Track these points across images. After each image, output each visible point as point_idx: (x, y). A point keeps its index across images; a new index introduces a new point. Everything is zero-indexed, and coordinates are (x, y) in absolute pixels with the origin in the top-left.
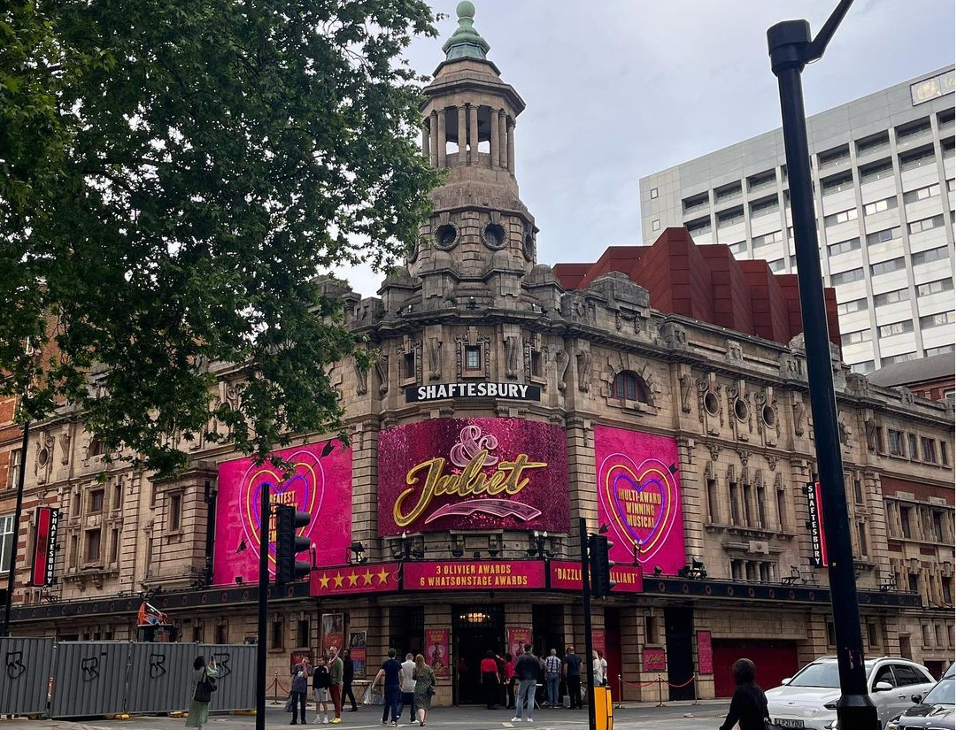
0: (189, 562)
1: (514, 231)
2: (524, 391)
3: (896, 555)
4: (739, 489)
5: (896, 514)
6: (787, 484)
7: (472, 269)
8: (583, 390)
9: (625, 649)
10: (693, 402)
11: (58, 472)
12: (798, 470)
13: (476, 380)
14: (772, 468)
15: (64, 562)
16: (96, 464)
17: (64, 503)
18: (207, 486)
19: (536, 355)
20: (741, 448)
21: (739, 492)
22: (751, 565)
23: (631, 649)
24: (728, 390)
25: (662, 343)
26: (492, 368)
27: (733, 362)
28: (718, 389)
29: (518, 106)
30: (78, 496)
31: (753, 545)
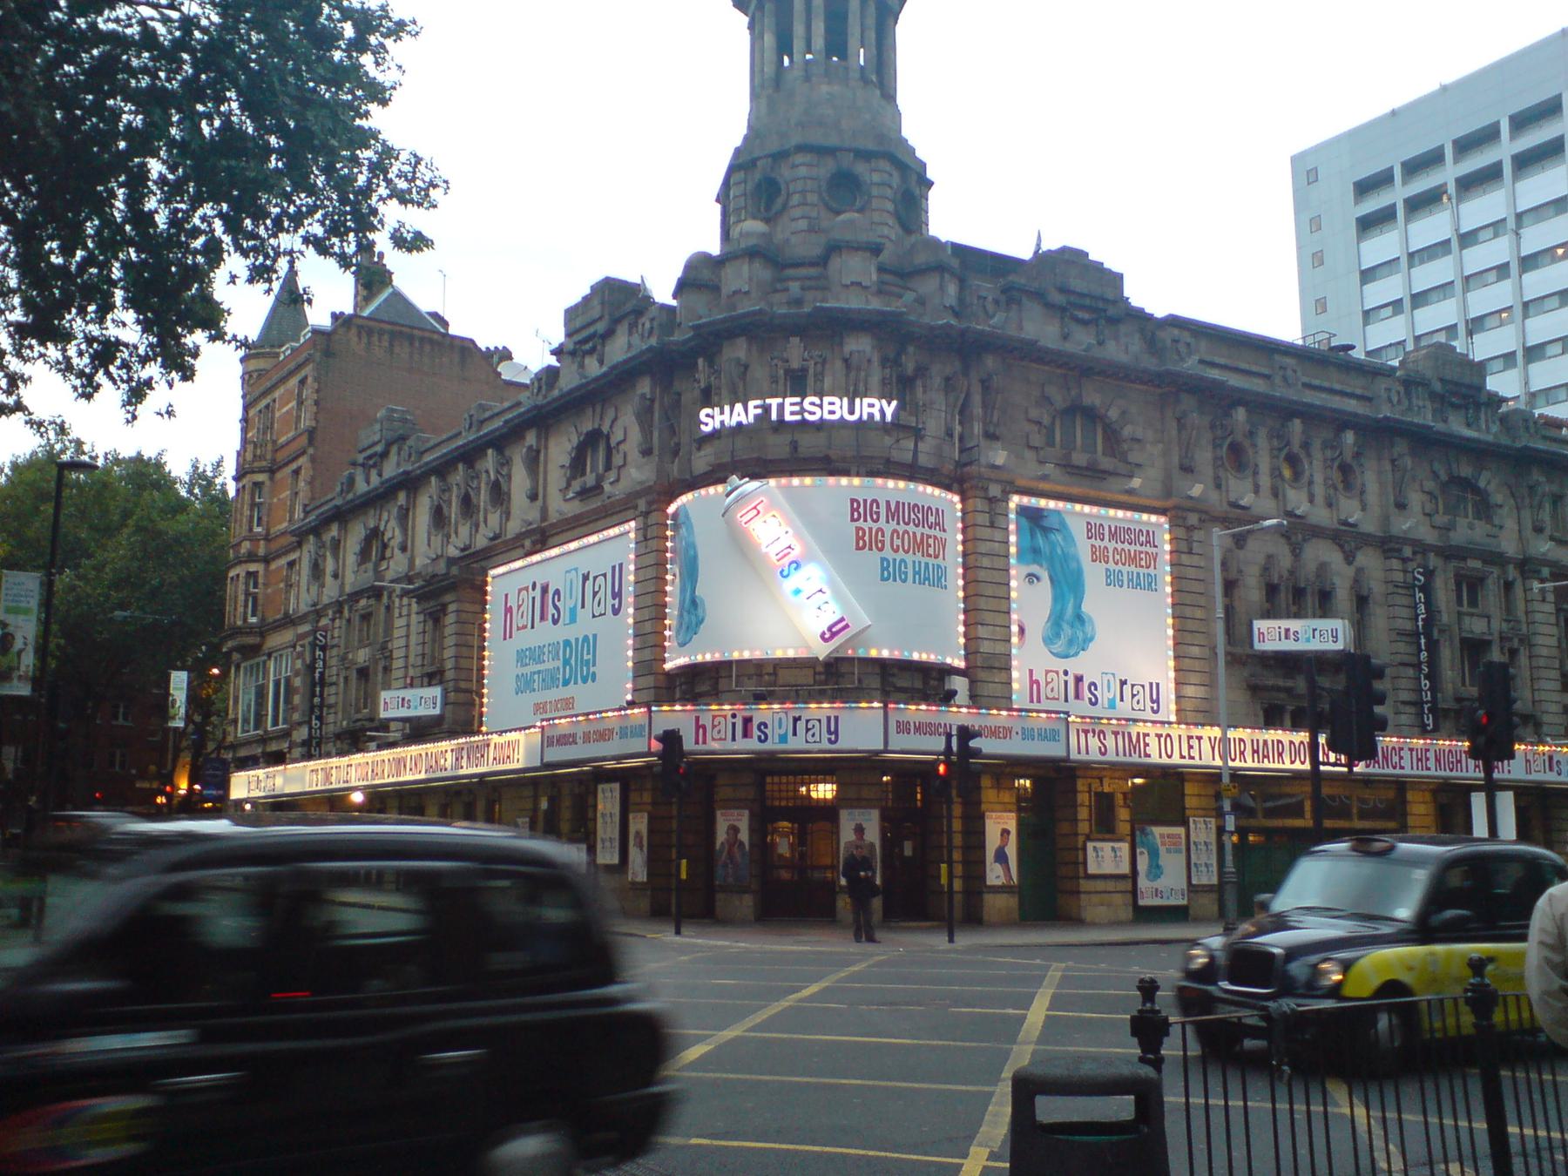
1: (873, 175)
4: (1283, 595)
6: (1376, 587)
8: (991, 436)
10: (1204, 457)
11: (331, 591)
12: (1396, 564)
14: (1349, 558)
16: (366, 578)
24: (1270, 437)
25: (1150, 363)
28: (1251, 434)
30: (349, 621)
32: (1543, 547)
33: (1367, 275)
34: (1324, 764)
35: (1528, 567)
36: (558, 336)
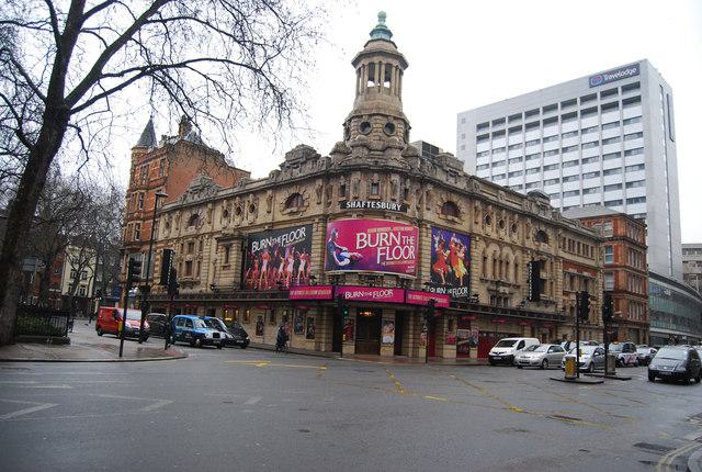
5: (568, 279)
9: (404, 340)
10: (480, 219)
17: (176, 248)
20: (500, 243)
21: (498, 263)
29: (405, 65)
31: (501, 289)
32: (561, 253)
33: (479, 155)
34: (185, 284)
35: (557, 258)
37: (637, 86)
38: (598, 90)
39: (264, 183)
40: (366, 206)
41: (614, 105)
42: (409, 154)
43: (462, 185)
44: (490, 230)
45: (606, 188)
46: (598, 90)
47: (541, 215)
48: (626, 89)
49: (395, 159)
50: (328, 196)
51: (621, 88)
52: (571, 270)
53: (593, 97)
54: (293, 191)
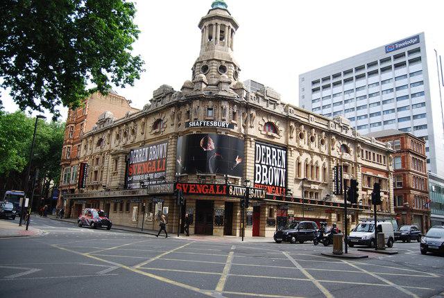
0: (118, 182)
2: (227, 125)
3: (365, 193)
5: (366, 179)
6: (327, 166)
7: (215, 81)
9: (233, 224)
10: (294, 135)
13: (210, 120)
15: (89, 180)
17: (89, 162)
18: (126, 157)
19: (234, 113)
20: (310, 152)
21: (310, 168)
22: (311, 193)
23: (263, 216)
25: (285, 114)
26: (217, 117)
27: (311, 123)
29: (236, 26)
31: (313, 186)
33: (313, 101)
36: (152, 97)
37: (418, 50)
38: (391, 54)
39: (135, 115)
40: (202, 125)
41: (403, 64)
42: (239, 89)
43: (279, 110)
44: (303, 144)
45: (399, 120)
46: (391, 54)
47: (344, 133)
48: (410, 53)
49: (227, 91)
50: (179, 119)
51: (407, 52)
52: (368, 173)
53: (388, 59)
54: (157, 117)
